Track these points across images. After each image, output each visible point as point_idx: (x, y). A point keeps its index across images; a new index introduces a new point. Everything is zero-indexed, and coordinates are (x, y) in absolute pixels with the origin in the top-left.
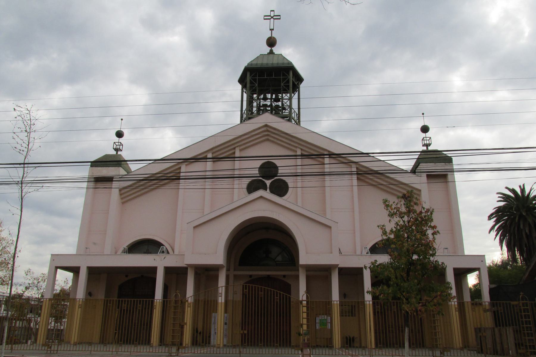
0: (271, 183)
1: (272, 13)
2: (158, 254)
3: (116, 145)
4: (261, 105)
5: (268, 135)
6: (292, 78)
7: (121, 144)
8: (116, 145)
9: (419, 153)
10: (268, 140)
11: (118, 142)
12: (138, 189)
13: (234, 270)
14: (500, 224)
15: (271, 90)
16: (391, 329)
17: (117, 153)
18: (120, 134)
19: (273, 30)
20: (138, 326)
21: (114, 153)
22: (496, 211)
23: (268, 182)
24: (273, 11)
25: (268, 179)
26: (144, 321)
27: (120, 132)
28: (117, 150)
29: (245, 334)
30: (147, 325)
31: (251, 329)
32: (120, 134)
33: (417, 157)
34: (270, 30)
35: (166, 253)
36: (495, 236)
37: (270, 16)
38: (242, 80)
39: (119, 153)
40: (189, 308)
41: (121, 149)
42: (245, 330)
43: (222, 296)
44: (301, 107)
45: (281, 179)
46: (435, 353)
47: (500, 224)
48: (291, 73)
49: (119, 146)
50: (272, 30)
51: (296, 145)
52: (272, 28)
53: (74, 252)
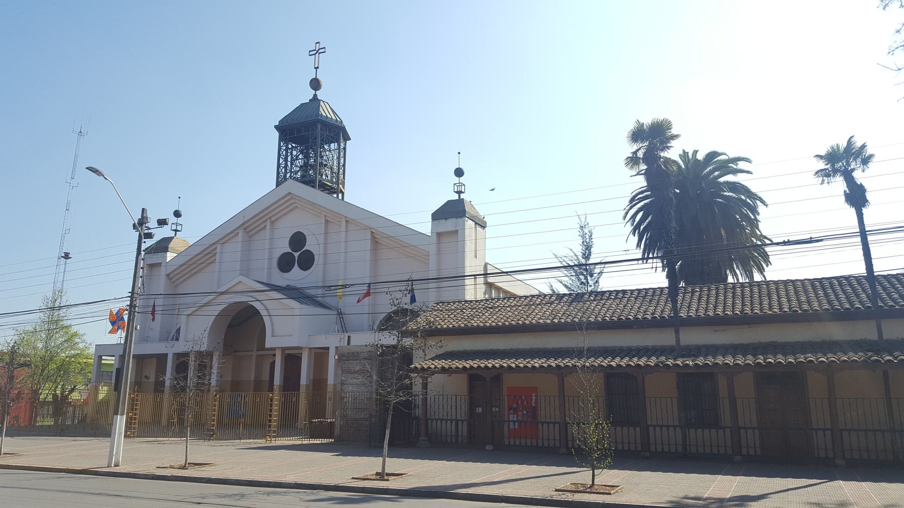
0: (295, 257)
10: (296, 207)
12: (205, 264)
18: (459, 173)
19: (318, 68)
21: (455, 197)
22: (742, 266)
23: (296, 255)
24: (319, 43)
25: (296, 252)
26: (261, 422)
30: (260, 425)
31: (290, 421)
32: (459, 173)
34: (315, 68)
37: (315, 50)
39: (462, 196)
40: (330, 401)
45: (300, 251)
46: (816, 434)
48: (319, 126)
49: (460, 187)
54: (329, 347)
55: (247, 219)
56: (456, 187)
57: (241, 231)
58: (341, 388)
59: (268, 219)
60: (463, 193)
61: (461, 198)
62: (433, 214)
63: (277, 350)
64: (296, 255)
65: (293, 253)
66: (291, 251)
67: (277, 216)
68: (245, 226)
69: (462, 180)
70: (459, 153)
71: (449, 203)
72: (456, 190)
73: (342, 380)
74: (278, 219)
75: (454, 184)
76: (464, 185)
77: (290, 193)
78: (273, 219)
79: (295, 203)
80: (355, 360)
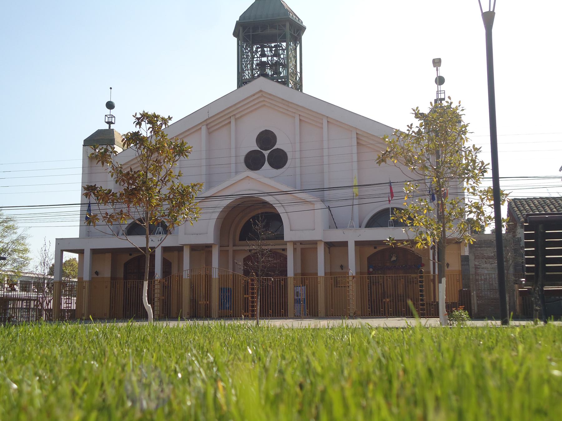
2: (155, 235)
3: (108, 117)
6: (290, 30)
8: (108, 117)
10: (264, 105)
11: (110, 115)
13: (234, 245)
16: (399, 298)
17: (110, 127)
20: (376, 302)
21: (106, 127)
23: (266, 153)
27: (111, 103)
28: (110, 123)
29: (208, 304)
32: (110, 105)
33: (221, 210)
35: (163, 234)
38: (236, 34)
41: (114, 122)
42: (208, 301)
49: (111, 118)
51: (294, 111)
53: (78, 237)
54: (347, 242)
55: (212, 116)
56: (107, 118)
57: (204, 128)
58: (476, 272)
59: (233, 116)
60: (113, 123)
61: (111, 128)
62: (85, 141)
63: (288, 243)
64: (266, 153)
65: (262, 151)
66: (260, 150)
67: (243, 113)
68: (208, 122)
69: (113, 112)
70: (111, 88)
71: (99, 133)
72: (107, 121)
73: (475, 265)
74: (241, 117)
75: (106, 115)
76: (114, 117)
77: (261, 91)
78: (237, 116)
79: (264, 101)
80: (489, 247)
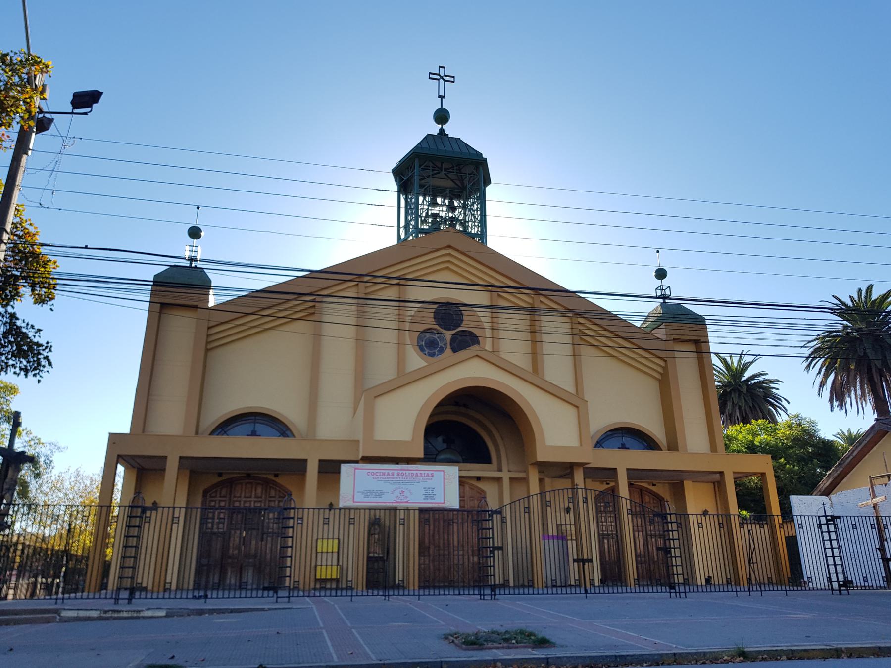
1: (442, 70)
4: (430, 214)
5: (449, 262)
7: (659, 288)
9: (435, 306)
10: (447, 268)
14: (858, 382)
15: (448, 192)
24: (444, 68)
34: (439, 97)
36: (829, 404)
43: (178, 523)
44: (397, 208)
47: (858, 382)
50: (442, 97)
52: (442, 94)
